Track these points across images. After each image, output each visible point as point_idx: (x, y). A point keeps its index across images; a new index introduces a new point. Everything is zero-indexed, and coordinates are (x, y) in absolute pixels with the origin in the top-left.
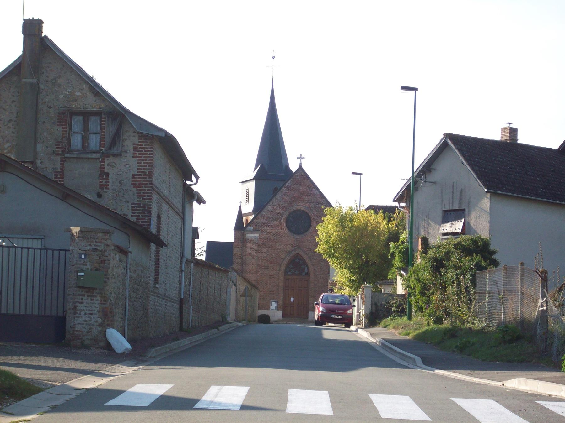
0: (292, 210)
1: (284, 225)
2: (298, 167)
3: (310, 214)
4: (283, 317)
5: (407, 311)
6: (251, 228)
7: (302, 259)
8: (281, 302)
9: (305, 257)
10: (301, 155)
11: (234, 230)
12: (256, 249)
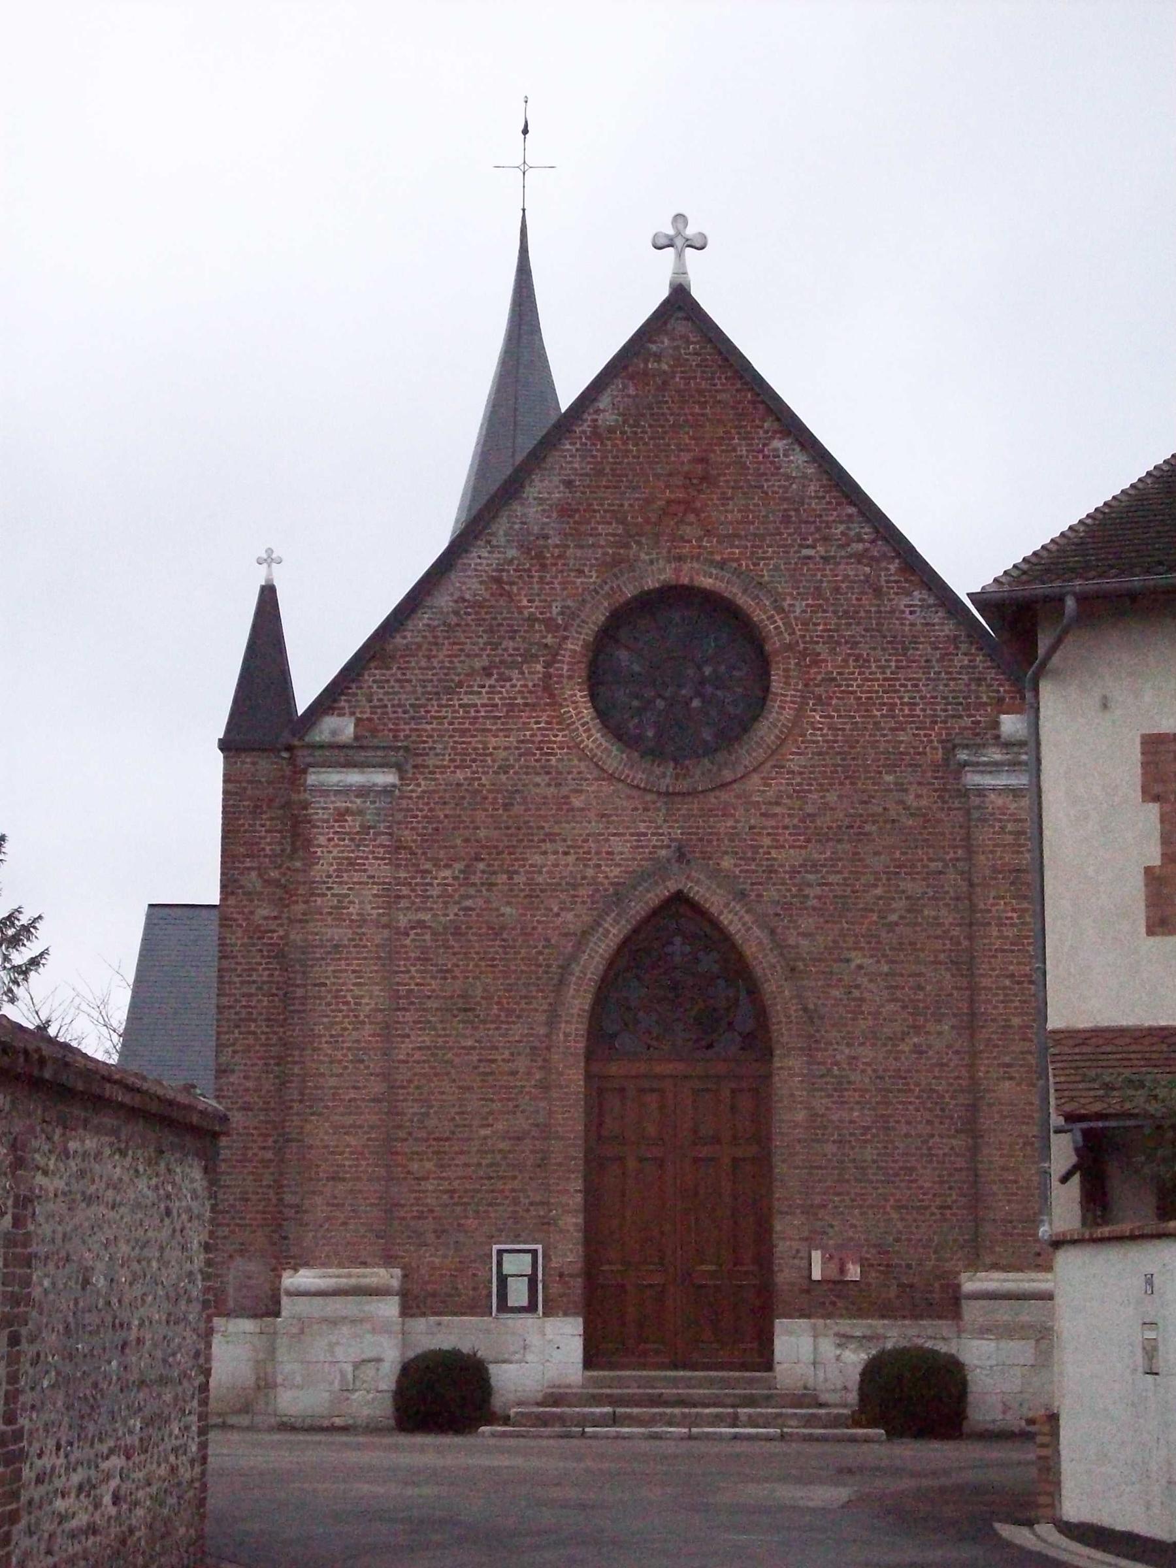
0: (629, 592)
1: (577, 704)
2: (664, 293)
3: (758, 616)
4: (589, 1362)
5: (1106, 1231)
6: (340, 727)
7: (715, 937)
8: (570, 1255)
9: (734, 920)
10: (680, 219)
11: (225, 745)
12: (383, 871)
